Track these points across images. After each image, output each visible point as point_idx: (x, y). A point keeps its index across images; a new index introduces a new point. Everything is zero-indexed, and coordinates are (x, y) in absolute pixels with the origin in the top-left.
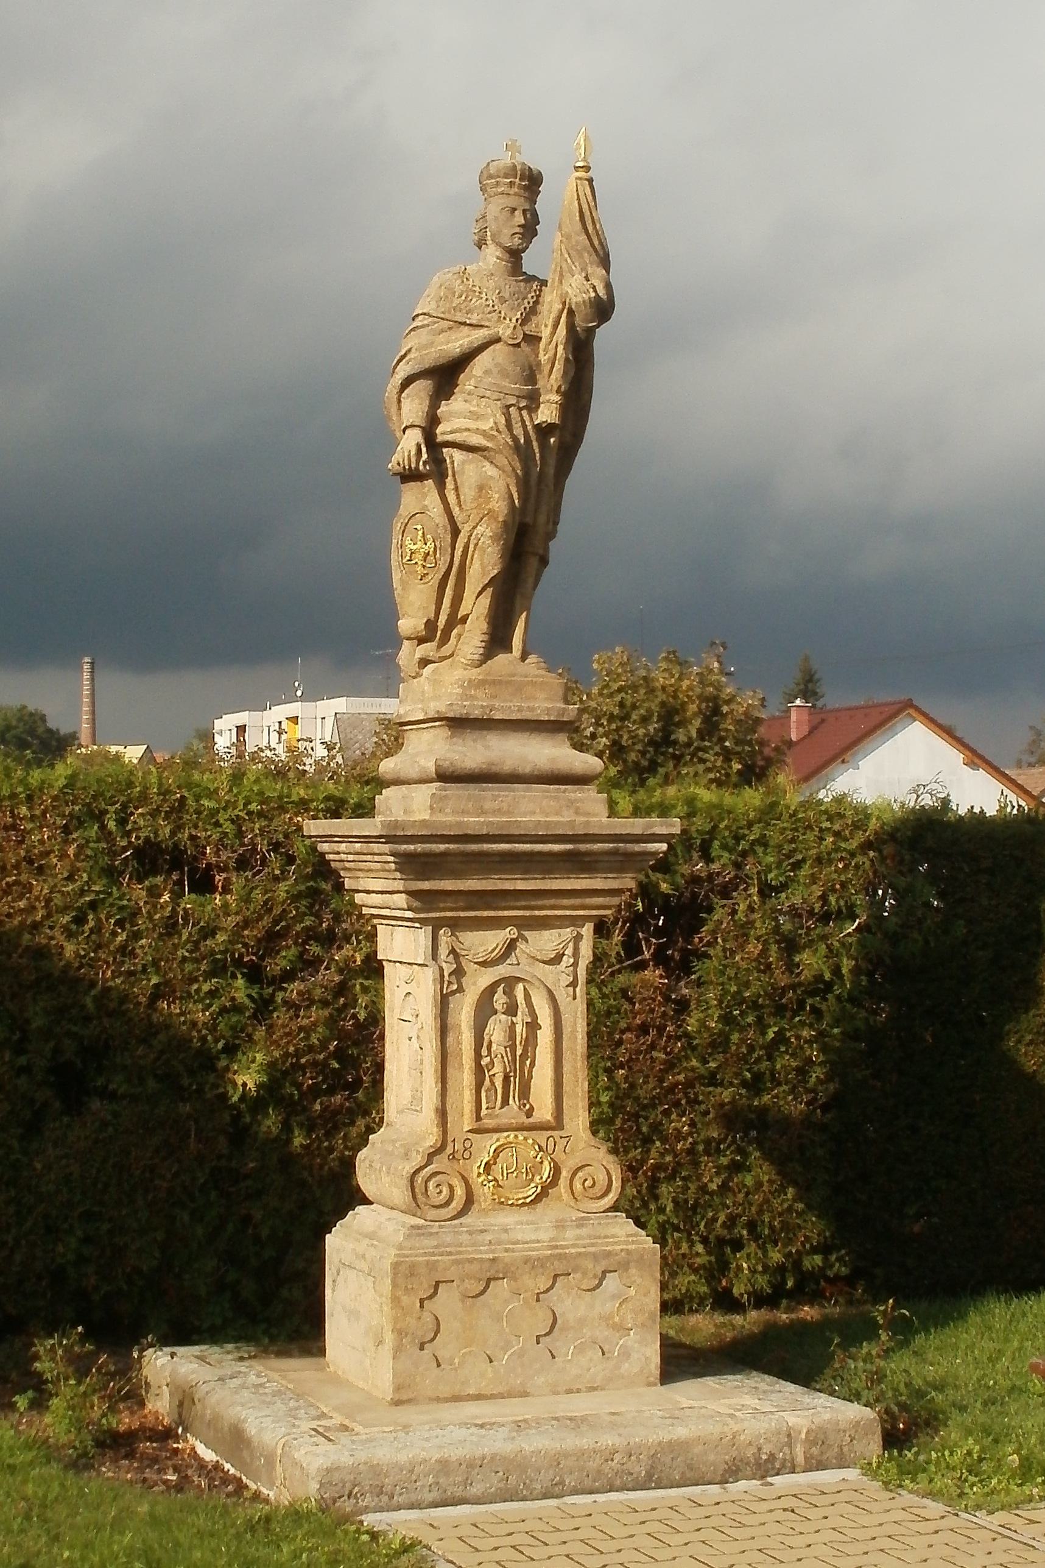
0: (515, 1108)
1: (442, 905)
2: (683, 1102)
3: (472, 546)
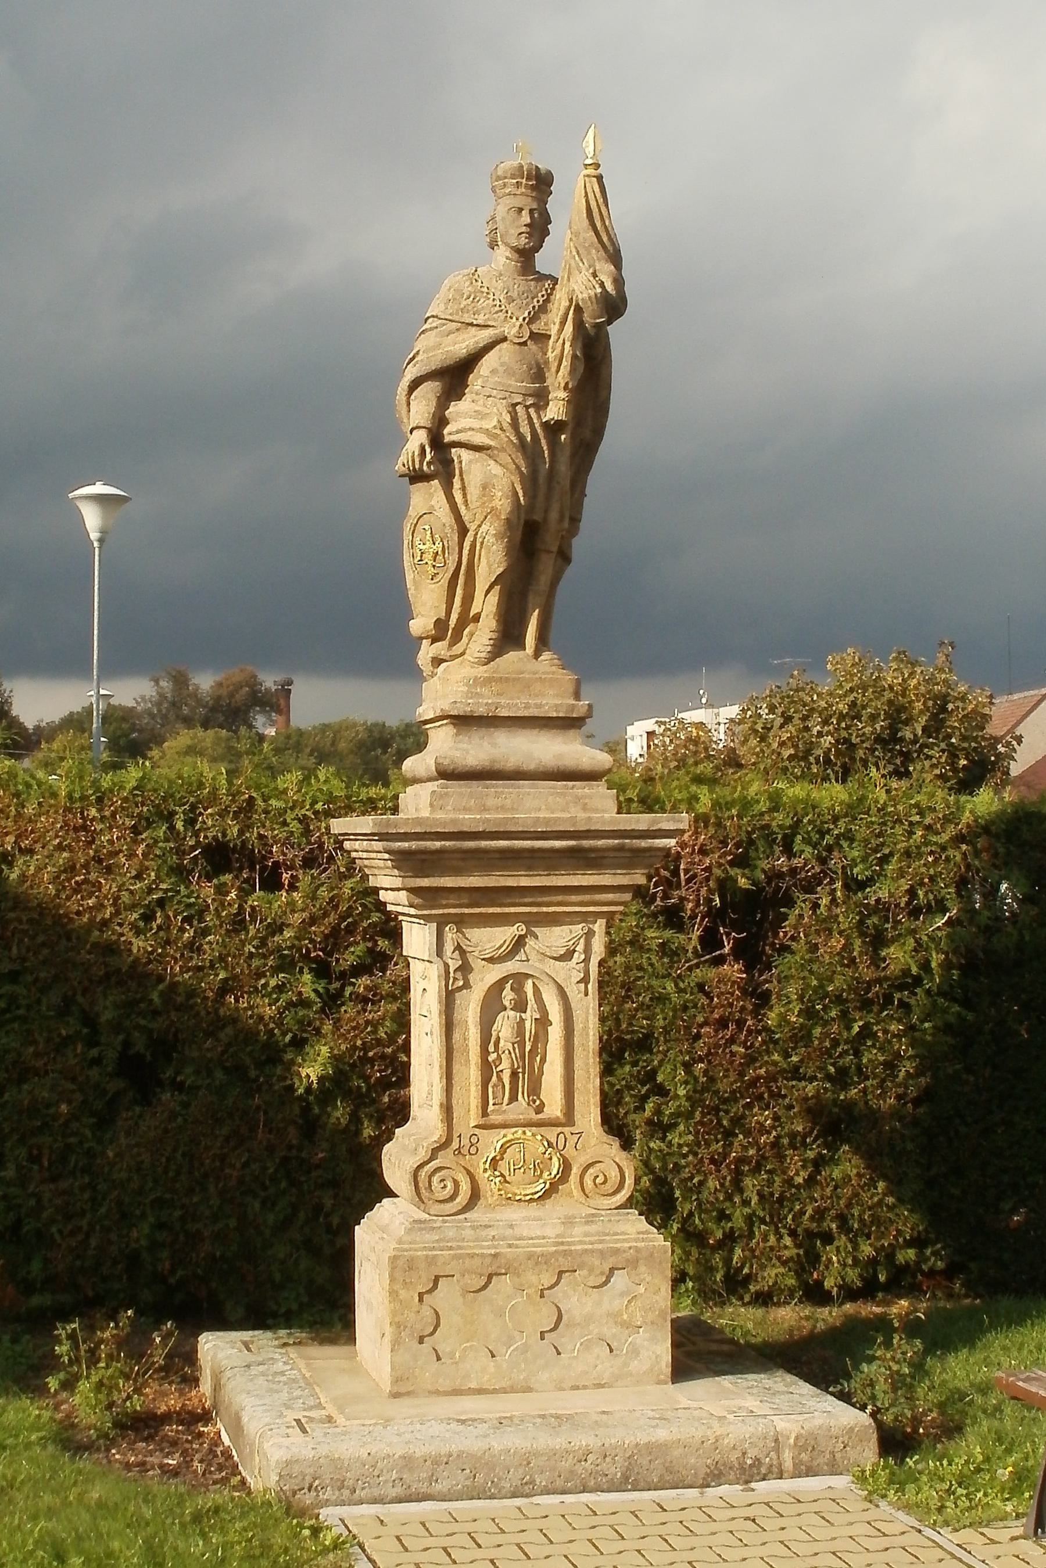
0: (524, 1104)
1: (444, 902)
2: (766, 1095)
3: (478, 545)
